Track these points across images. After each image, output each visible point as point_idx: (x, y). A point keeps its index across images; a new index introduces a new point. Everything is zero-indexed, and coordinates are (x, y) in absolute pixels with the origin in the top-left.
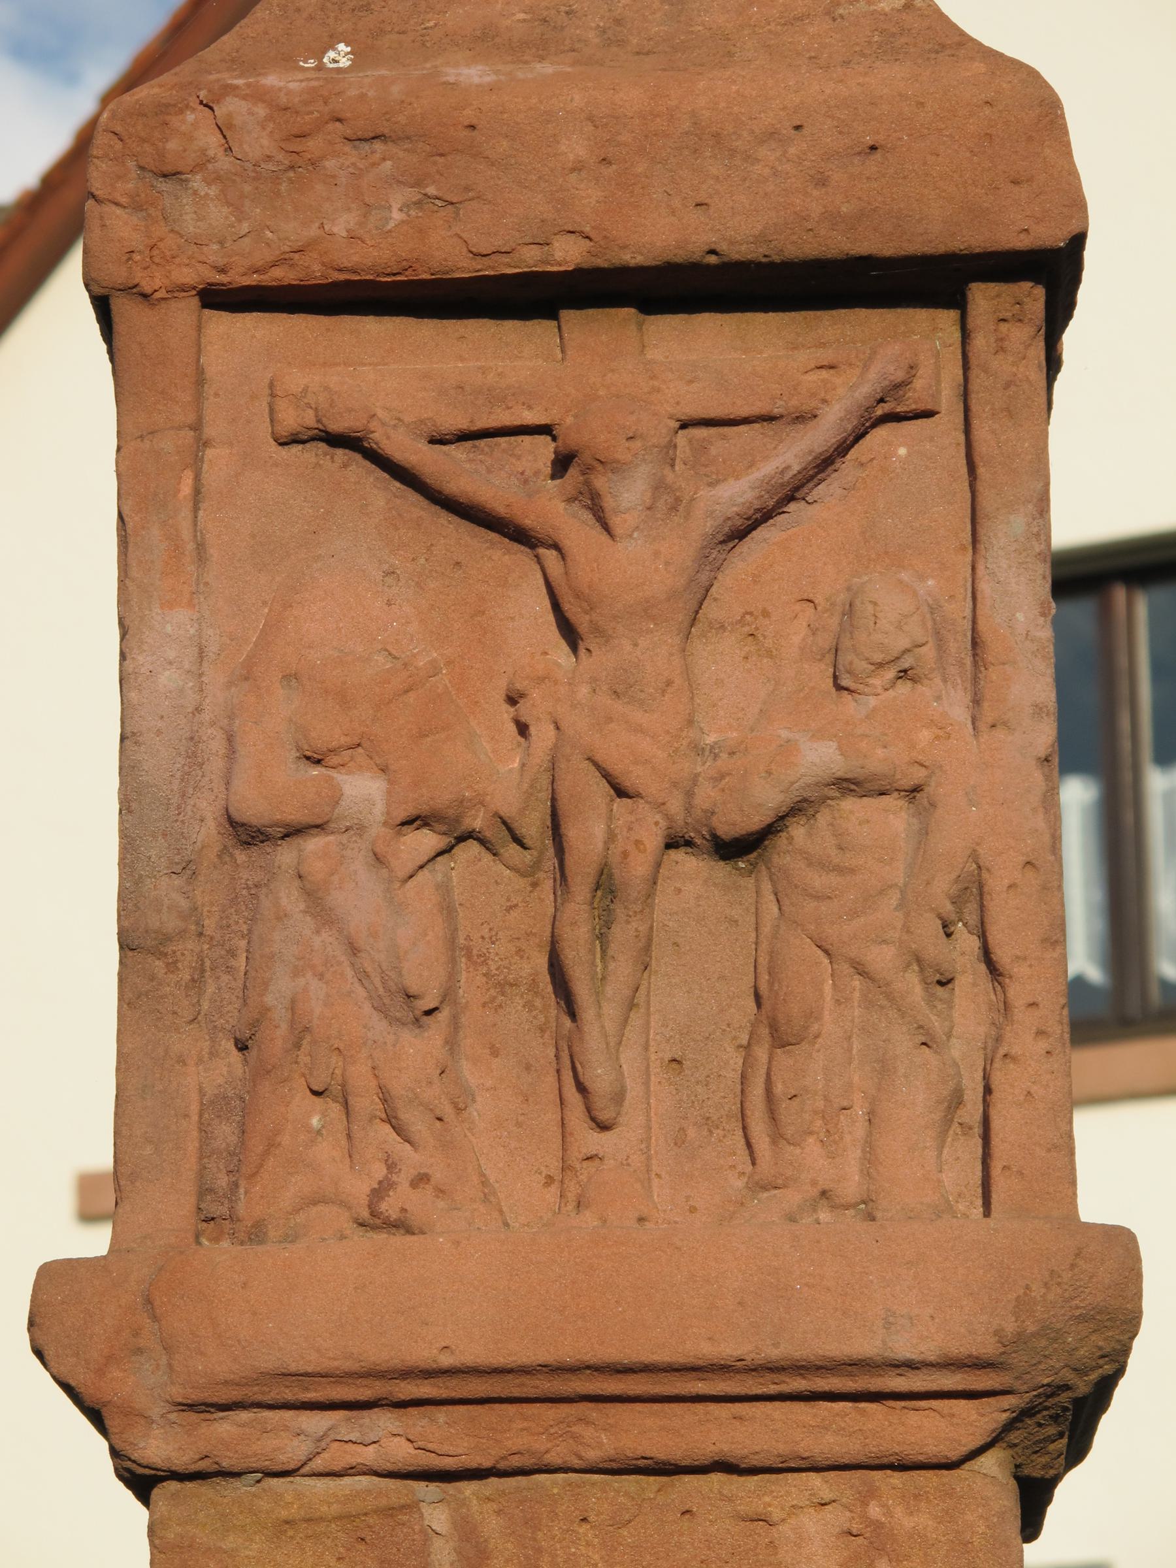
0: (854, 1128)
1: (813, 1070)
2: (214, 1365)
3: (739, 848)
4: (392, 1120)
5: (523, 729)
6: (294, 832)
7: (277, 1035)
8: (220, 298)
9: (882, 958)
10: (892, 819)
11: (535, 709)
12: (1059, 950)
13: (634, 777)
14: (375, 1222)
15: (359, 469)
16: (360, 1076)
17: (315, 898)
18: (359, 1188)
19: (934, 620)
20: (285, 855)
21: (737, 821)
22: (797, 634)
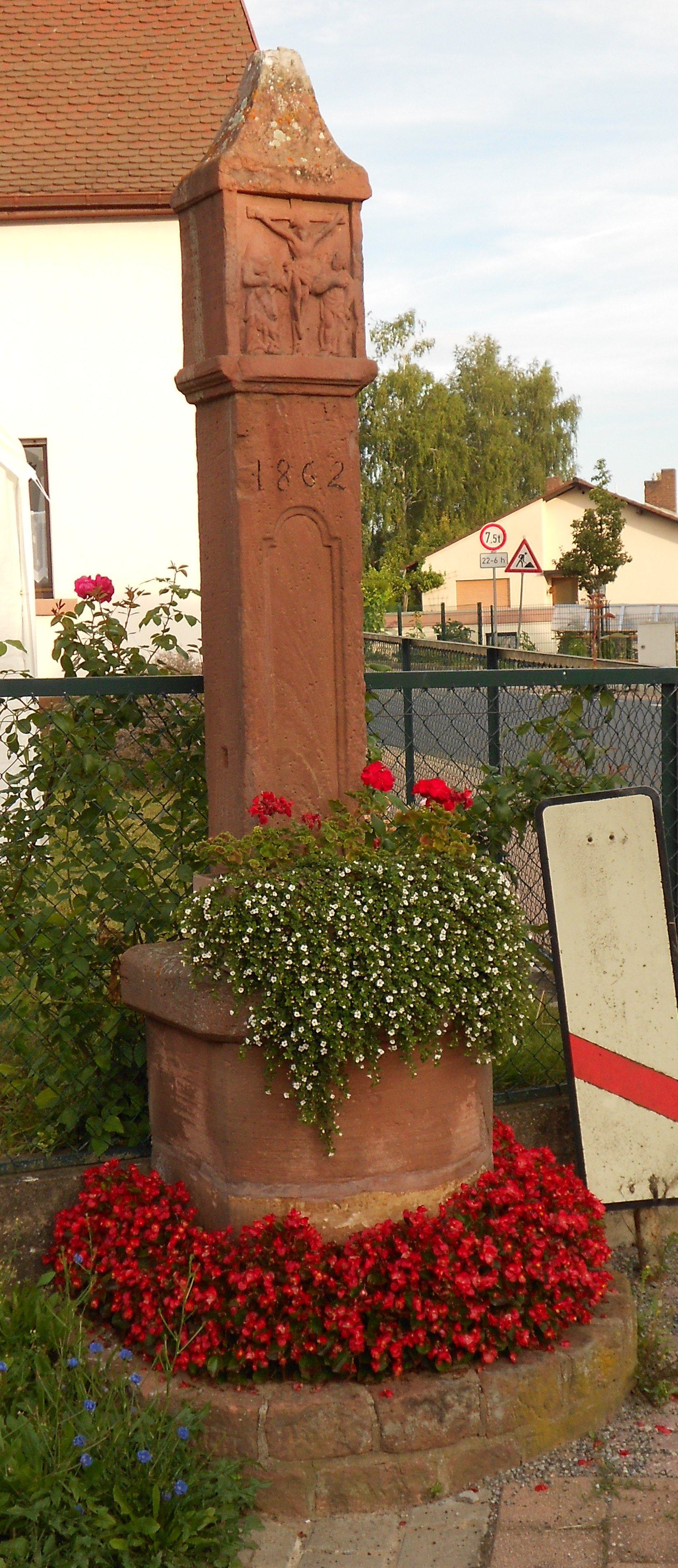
0: (335, 342)
1: (330, 332)
2: (250, 374)
3: (318, 295)
4: (271, 337)
5: (286, 271)
6: (255, 286)
7: (253, 321)
8: (239, 192)
9: (341, 315)
10: (339, 292)
11: (289, 268)
12: (565, 1098)
13: (306, 281)
14: (268, 353)
15: (260, 224)
16: (266, 328)
17: (258, 297)
18: (266, 347)
19: (470, 655)
20: (253, 290)
21: (319, 290)
22: (325, 260)
